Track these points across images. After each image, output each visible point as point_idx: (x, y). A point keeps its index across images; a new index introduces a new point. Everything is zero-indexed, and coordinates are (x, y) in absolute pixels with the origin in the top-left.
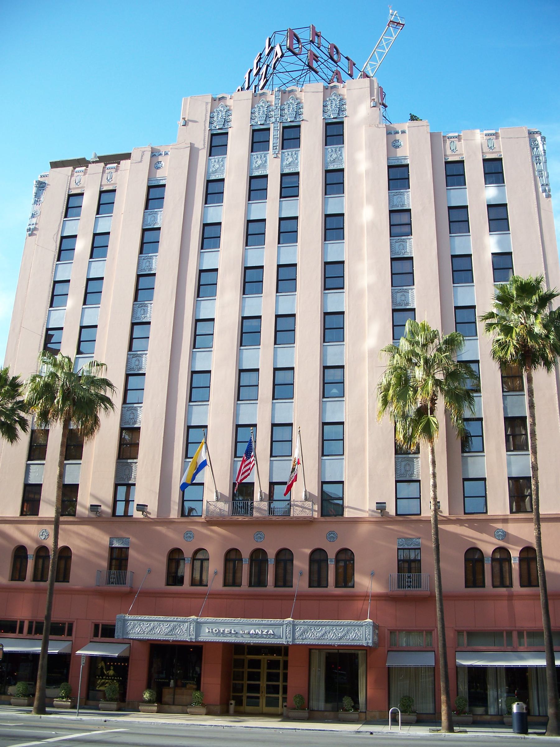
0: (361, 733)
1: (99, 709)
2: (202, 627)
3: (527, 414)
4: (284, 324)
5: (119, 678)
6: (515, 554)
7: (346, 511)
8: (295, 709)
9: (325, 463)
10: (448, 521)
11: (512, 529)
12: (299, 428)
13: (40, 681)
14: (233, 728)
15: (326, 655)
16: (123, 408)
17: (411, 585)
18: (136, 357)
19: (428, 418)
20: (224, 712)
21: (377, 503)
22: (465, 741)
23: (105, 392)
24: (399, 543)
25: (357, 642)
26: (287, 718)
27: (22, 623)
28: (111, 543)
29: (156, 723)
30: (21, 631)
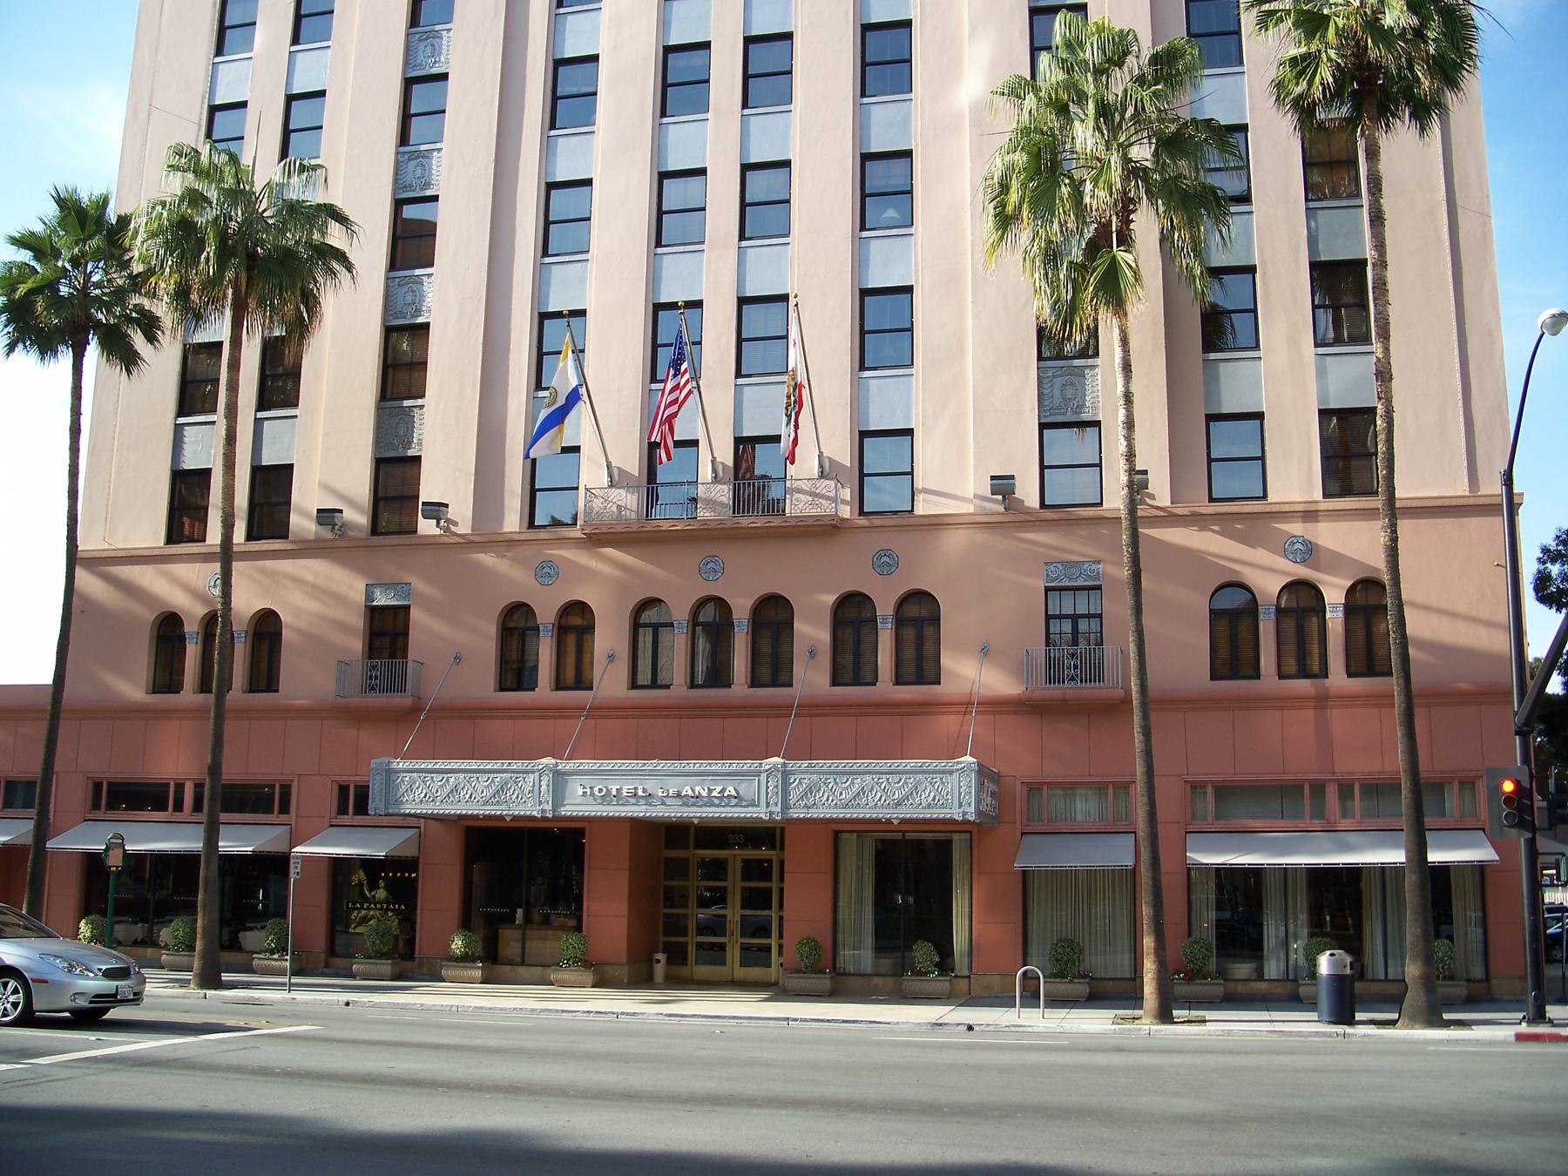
0: (945, 1027)
1: (352, 976)
2: (567, 782)
3: (1369, 254)
4: (765, 58)
5: (399, 907)
6: (1334, 595)
7: (919, 501)
8: (800, 971)
9: (868, 386)
10: (1168, 519)
11: (1328, 535)
12: (795, 297)
13: (204, 915)
14: (640, 1017)
15: (876, 846)
16: (389, 281)
17: (1077, 676)
18: (418, 157)
19: (1111, 255)
20: (641, 979)
21: (993, 478)
22: (1179, 1051)
23: (324, 234)
24: (1048, 575)
25: (938, 811)
26: (781, 992)
27: (180, 787)
28: (369, 596)
29: (461, 1007)
30: (179, 807)
